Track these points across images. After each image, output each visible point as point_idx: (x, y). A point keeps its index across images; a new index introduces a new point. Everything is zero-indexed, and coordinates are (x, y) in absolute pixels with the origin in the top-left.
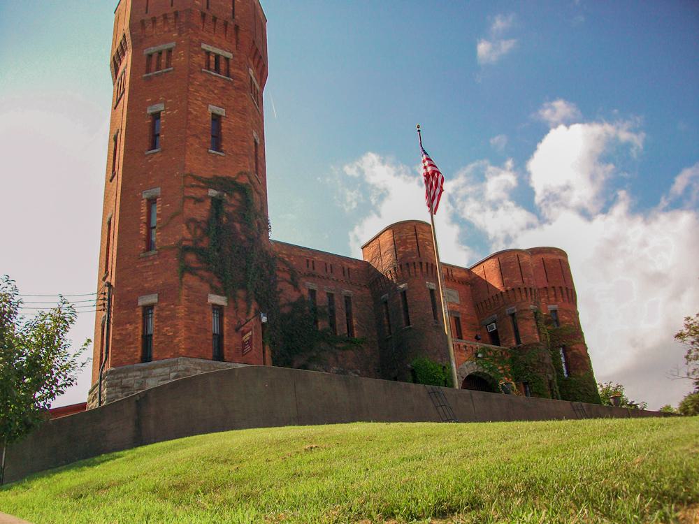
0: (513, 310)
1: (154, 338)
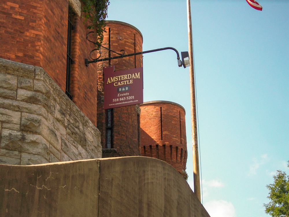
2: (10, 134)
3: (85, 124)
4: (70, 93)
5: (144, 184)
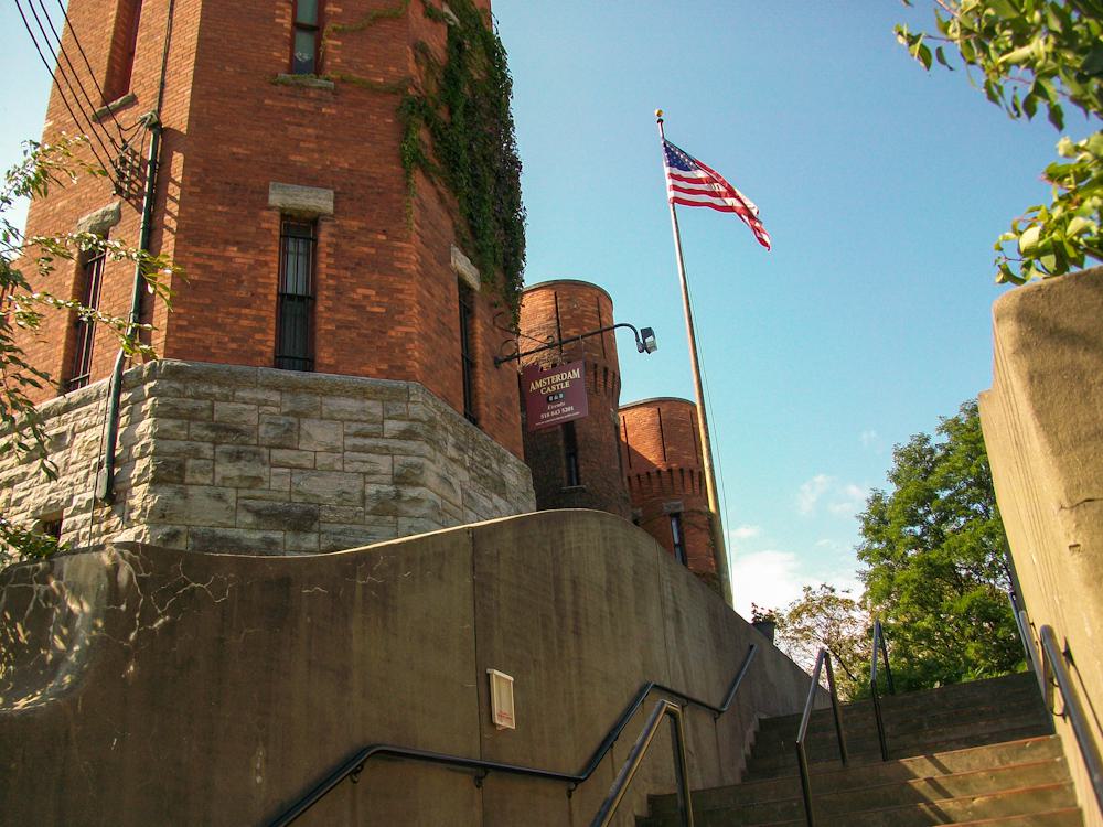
0: (678, 506)
1: (321, 308)
2: (378, 491)
3: (501, 460)
4: (472, 416)
5: (564, 552)
